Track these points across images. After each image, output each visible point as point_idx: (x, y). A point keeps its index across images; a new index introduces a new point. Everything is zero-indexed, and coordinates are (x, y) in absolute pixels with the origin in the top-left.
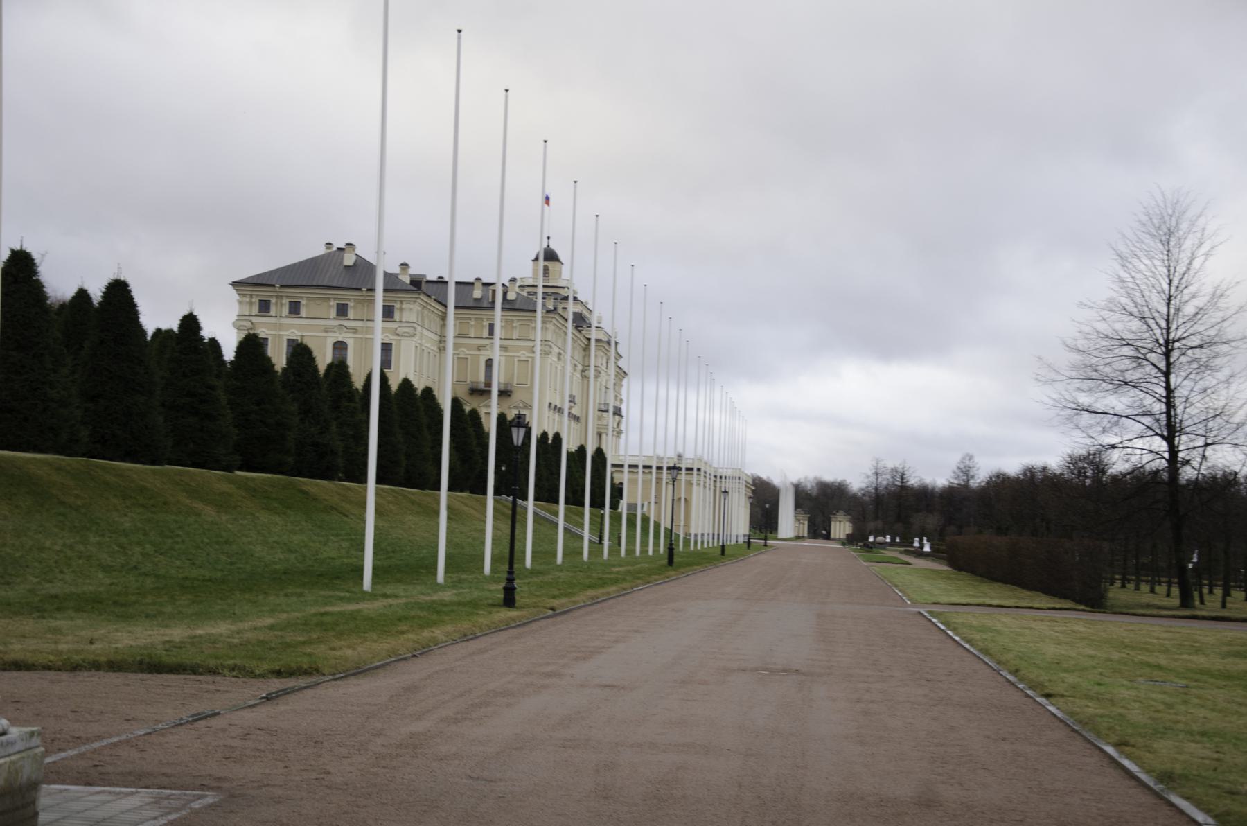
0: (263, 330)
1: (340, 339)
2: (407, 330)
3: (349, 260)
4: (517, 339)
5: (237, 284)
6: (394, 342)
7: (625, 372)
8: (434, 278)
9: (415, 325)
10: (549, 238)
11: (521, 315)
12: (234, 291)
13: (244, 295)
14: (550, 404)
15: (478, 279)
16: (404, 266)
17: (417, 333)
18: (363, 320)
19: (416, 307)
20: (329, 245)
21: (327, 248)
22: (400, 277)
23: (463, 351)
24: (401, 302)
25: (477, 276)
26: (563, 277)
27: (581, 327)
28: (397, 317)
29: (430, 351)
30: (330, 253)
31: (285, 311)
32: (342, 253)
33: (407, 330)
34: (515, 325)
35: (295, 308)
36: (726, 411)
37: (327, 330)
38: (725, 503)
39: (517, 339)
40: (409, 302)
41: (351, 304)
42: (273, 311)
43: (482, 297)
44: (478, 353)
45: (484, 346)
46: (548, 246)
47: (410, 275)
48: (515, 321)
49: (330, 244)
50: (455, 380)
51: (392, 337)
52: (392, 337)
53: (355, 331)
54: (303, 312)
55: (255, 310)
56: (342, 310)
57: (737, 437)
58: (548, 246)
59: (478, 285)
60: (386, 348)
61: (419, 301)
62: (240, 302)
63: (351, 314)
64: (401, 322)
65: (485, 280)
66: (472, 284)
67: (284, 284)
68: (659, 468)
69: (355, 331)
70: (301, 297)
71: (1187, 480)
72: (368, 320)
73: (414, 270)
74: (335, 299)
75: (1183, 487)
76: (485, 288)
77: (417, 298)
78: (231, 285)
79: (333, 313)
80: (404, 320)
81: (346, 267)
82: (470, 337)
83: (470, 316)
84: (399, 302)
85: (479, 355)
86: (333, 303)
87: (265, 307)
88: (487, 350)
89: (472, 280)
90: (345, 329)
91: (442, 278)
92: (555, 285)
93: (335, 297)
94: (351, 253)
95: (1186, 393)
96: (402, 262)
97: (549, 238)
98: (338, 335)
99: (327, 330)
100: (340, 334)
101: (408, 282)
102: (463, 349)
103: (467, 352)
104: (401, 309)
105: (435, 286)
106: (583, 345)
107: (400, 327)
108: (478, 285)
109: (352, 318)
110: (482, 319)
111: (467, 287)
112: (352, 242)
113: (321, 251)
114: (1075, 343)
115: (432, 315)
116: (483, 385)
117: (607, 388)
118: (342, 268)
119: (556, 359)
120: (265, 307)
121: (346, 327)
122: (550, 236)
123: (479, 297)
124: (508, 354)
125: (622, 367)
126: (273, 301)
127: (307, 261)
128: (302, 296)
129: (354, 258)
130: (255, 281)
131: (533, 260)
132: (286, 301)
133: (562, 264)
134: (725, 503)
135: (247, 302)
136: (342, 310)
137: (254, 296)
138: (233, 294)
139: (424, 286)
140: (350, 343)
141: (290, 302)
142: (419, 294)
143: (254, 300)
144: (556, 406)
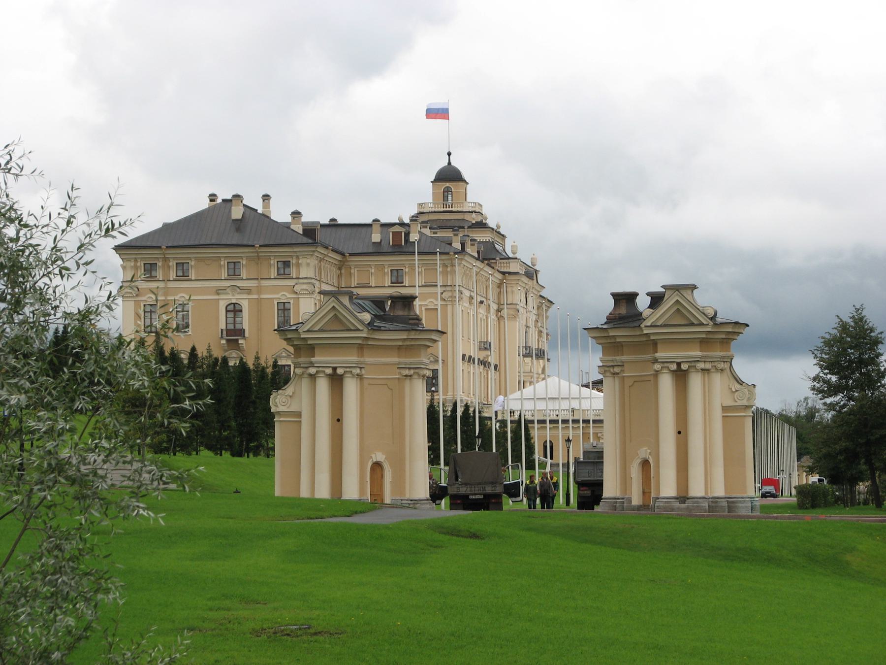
2: (305, 287)
3: (237, 213)
7: (549, 301)
8: (327, 222)
9: (313, 281)
10: (449, 154)
13: (129, 260)
14: (464, 356)
15: (376, 221)
16: (296, 214)
18: (258, 279)
19: (313, 262)
22: (292, 227)
24: (298, 257)
26: (468, 200)
27: (494, 259)
28: (294, 272)
31: (172, 275)
32: (228, 204)
33: (305, 287)
37: (218, 291)
38: (681, 433)
40: (305, 257)
42: (160, 274)
44: (217, 297)
46: (449, 163)
47: (303, 224)
48: (272, 258)
49: (215, 195)
53: (248, 291)
54: (193, 275)
56: (234, 274)
58: (449, 163)
59: (377, 227)
61: (316, 254)
64: (299, 278)
65: (383, 221)
66: (370, 225)
67: (170, 244)
68: (585, 421)
69: (248, 291)
70: (190, 258)
71: (812, 482)
72: (261, 279)
73: (306, 218)
74: (226, 258)
75: (332, 498)
76: (385, 229)
77: (314, 251)
78: (114, 249)
80: (300, 277)
82: (371, 287)
84: (294, 258)
87: (150, 268)
88: (228, 294)
89: (369, 221)
90: (239, 290)
91: (335, 220)
92: (459, 209)
94: (239, 206)
96: (264, 194)
97: (449, 154)
98: (230, 297)
99: (218, 291)
100: (233, 295)
104: (298, 265)
105: (329, 230)
106: (498, 282)
107: (297, 284)
110: (383, 267)
111: (364, 230)
113: (205, 204)
115: (329, 266)
117: (527, 327)
118: (231, 221)
119: (467, 305)
120: (150, 268)
121: (238, 287)
125: (545, 296)
126: (160, 264)
129: (242, 209)
130: (143, 244)
131: (431, 182)
132: (173, 263)
133: (467, 183)
134: (681, 433)
135: (132, 267)
136: (234, 274)
137: (139, 260)
139: (320, 236)
140: (245, 305)
142: (317, 247)
143: (139, 264)
144: (470, 357)
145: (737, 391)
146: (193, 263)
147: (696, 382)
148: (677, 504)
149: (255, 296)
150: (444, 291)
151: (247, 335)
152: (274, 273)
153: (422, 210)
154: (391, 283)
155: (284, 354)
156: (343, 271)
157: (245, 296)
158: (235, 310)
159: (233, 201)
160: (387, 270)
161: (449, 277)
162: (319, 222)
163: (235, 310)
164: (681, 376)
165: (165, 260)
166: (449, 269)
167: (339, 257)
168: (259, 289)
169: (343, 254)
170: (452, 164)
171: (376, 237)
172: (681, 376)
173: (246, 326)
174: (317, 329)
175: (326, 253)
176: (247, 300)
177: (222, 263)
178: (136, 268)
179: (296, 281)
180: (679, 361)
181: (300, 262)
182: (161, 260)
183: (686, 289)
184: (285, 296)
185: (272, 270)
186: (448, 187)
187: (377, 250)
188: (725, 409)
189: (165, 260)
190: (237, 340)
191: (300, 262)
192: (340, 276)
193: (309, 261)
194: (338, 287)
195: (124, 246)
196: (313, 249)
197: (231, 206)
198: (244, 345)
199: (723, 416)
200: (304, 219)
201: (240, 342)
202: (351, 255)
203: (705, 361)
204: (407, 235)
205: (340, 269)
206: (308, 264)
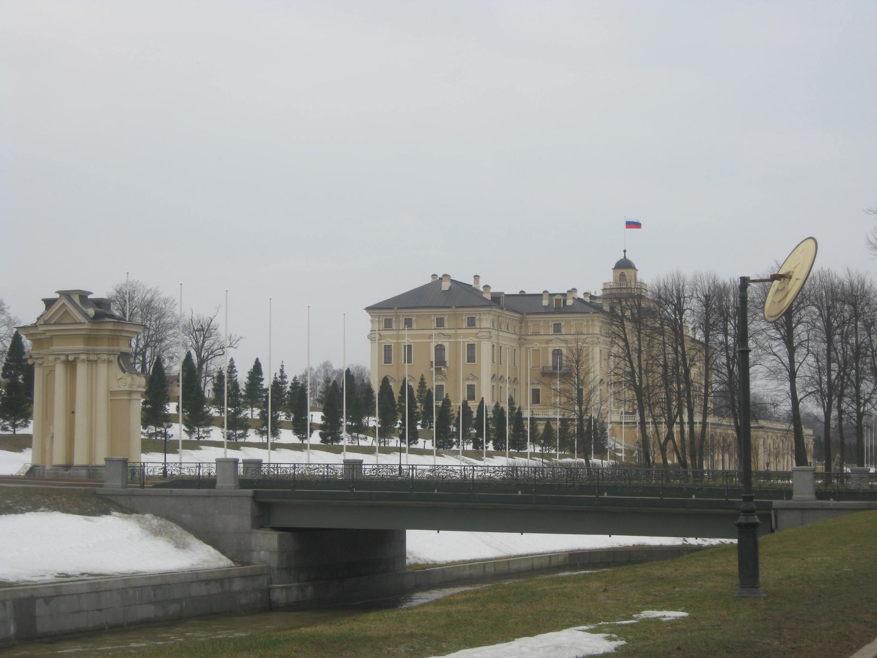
0: (536, 343)
1: (440, 343)
2: (484, 334)
3: (446, 286)
4: (531, 335)
5: (368, 309)
6: (476, 343)
8: (518, 293)
10: (625, 251)
11: (568, 316)
12: (368, 313)
15: (545, 292)
17: (493, 336)
19: (490, 317)
20: (434, 276)
21: (433, 278)
23: (536, 345)
25: (544, 290)
28: (477, 325)
29: (515, 348)
30: (435, 281)
31: (402, 325)
33: (484, 334)
34: (572, 324)
35: (408, 323)
36: (98, 330)
39: (531, 335)
41: (446, 318)
42: (394, 326)
43: (549, 305)
44: (429, 341)
45: (551, 340)
46: (625, 257)
47: (492, 293)
48: (551, 322)
50: (531, 366)
51: (475, 340)
52: (475, 340)
53: (449, 336)
54: (414, 326)
55: (382, 326)
56: (440, 323)
57: (127, 329)
58: (625, 257)
59: (545, 296)
60: (471, 348)
61: (491, 312)
62: (372, 322)
63: (446, 325)
65: (551, 292)
66: (541, 295)
69: (449, 336)
73: (494, 290)
77: (490, 311)
78: (365, 309)
79: (434, 325)
80: (482, 327)
81: (443, 291)
82: (541, 335)
83: (570, 319)
84: (478, 315)
85: (430, 342)
86: (434, 318)
87: (388, 324)
88: (553, 343)
89: (541, 292)
93: (466, 313)
95: (799, 332)
96: (475, 274)
97: (625, 251)
98: (555, 345)
99: (430, 337)
100: (440, 339)
101: (490, 299)
102: (536, 343)
103: (539, 346)
104: (480, 320)
107: (479, 332)
108: (545, 296)
109: (447, 328)
112: (489, 285)
113: (429, 280)
114: (5, 348)
116: (551, 369)
122: (626, 249)
123: (547, 305)
124: (451, 340)
126: (394, 319)
127: (405, 293)
128: (413, 313)
132: (402, 319)
136: (440, 323)
138: (367, 317)
139: (502, 301)
140: (447, 345)
141: (405, 319)
143: (381, 319)
145: (121, 378)
146: (542, 324)
147: (82, 370)
148: (62, 472)
149: (453, 340)
150: (587, 338)
151: (448, 365)
152: (465, 324)
153: (605, 287)
154: (554, 332)
155: (471, 378)
156: (523, 325)
157: (447, 340)
158: (440, 349)
159: (443, 279)
160: (551, 324)
161: (590, 329)
162: (503, 293)
163: (440, 349)
164: (71, 365)
165: (397, 316)
166: (590, 323)
167: (518, 316)
168: (457, 336)
169: (522, 314)
170: (627, 258)
171: (545, 302)
172: (71, 365)
173: (447, 359)
174: (53, 322)
175: (502, 312)
176: (448, 343)
177: (433, 318)
178: (379, 322)
179: (587, 336)
180: (67, 353)
181: (482, 317)
182: (395, 316)
183: (74, 294)
184: (472, 340)
185: (464, 323)
186: (623, 273)
187: (547, 311)
188: (112, 393)
189: (397, 316)
190: (441, 368)
191: (482, 317)
192: (521, 328)
193: (487, 317)
194: (520, 335)
195: (374, 308)
196: (490, 309)
197: (442, 282)
198: (446, 371)
199: (111, 400)
200: (492, 291)
201: (443, 369)
202: (528, 314)
203: (94, 354)
204: (565, 301)
205: (521, 323)
206: (487, 320)
